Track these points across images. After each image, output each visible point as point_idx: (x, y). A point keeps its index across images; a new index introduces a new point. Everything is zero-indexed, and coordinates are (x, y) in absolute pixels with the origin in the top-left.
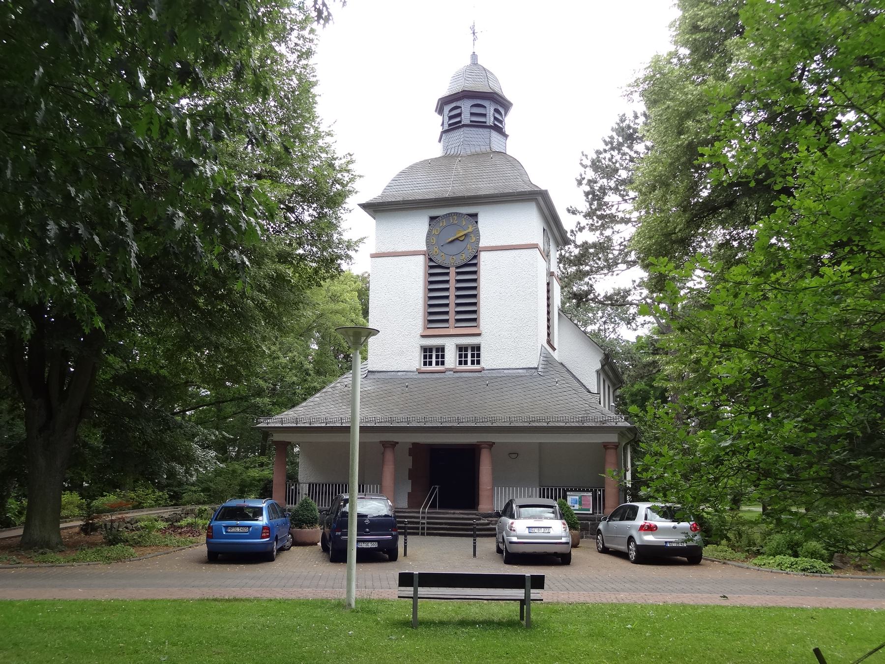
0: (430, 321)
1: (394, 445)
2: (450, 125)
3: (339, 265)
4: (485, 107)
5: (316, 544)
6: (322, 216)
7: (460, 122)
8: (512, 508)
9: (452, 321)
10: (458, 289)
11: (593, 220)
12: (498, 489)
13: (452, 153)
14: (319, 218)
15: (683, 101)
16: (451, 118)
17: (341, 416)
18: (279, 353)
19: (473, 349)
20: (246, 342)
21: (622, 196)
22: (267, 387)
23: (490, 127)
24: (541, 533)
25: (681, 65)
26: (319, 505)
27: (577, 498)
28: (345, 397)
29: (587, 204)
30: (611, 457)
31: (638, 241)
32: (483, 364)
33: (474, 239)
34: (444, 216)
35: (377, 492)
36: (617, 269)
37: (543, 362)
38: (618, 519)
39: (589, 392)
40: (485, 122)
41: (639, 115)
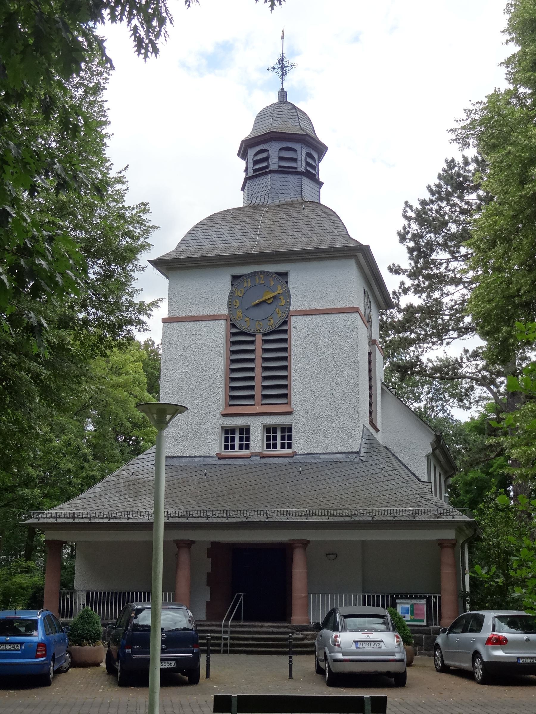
0: (233, 398)
1: (190, 544)
2: (255, 171)
3: (129, 331)
4: (295, 151)
5: (98, 665)
6: (108, 275)
7: (267, 167)
8: (335, 618)
9: (258, 397)
10: (265, 360)
11: (419, 280)
12: (314, 597)
13: (258, 202)
14: (105, 276)
15: (526, 146)
16: (256, 162)
17: (127, 510)
18: (51, 435)
19: (241, 431)
20: (16, 422)
21: (452, 253)
22: (38, 475)
23: (301, 173)
24: (369, 648)
25: (522, 106)
26: (103, 618)
27: (408, 606)
28: (131, 487)
29: (412, 263)
30: (447, 557)
31: (476, 306)
32: (294, 448)
33: (283, 302)
34: (248, 274)
35: (170, 600)
36: (448, 337)
37: (366, 446)
38: (460, 630)
39: (419, 480)
40: (296, 168)
41: (470, 160)
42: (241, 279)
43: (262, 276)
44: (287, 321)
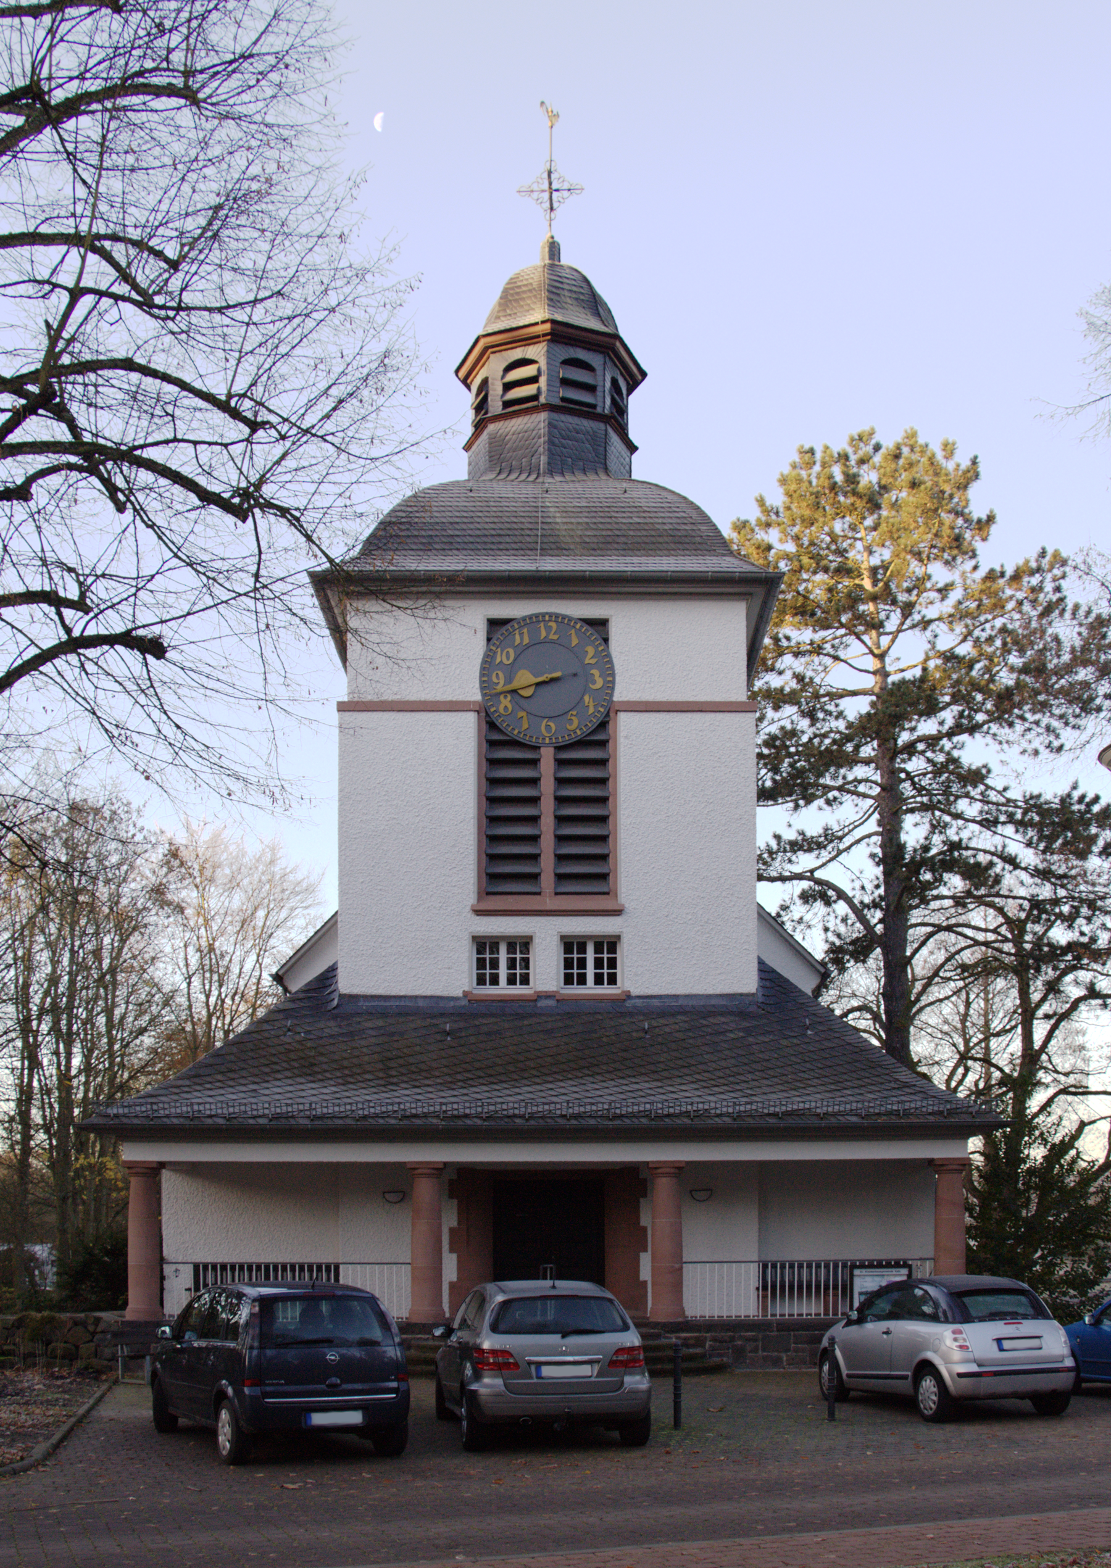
2: (507, 404)
7: (535, 398)
34: (524, 619)
40: (594, 406)
42: (508, 626)
43: (553, 625)
44: (608, 722)
